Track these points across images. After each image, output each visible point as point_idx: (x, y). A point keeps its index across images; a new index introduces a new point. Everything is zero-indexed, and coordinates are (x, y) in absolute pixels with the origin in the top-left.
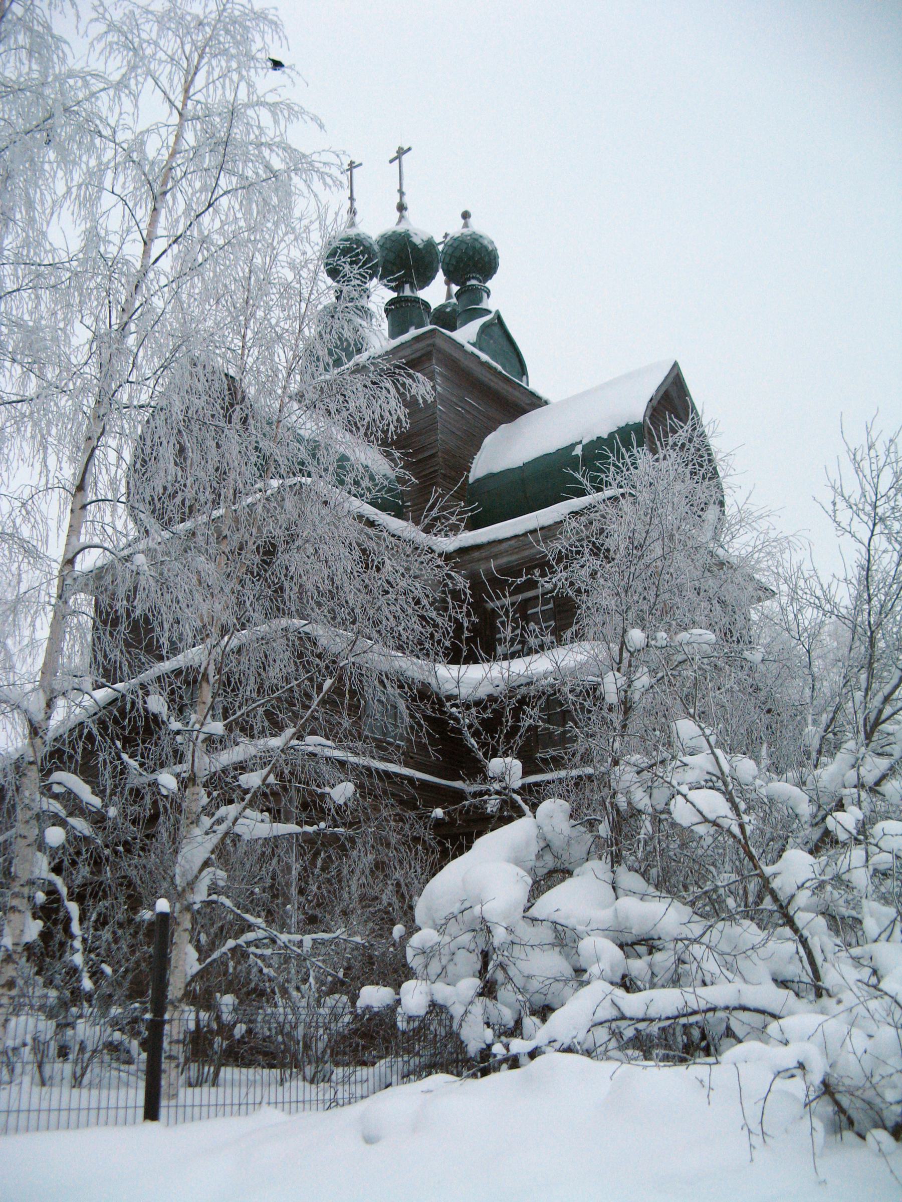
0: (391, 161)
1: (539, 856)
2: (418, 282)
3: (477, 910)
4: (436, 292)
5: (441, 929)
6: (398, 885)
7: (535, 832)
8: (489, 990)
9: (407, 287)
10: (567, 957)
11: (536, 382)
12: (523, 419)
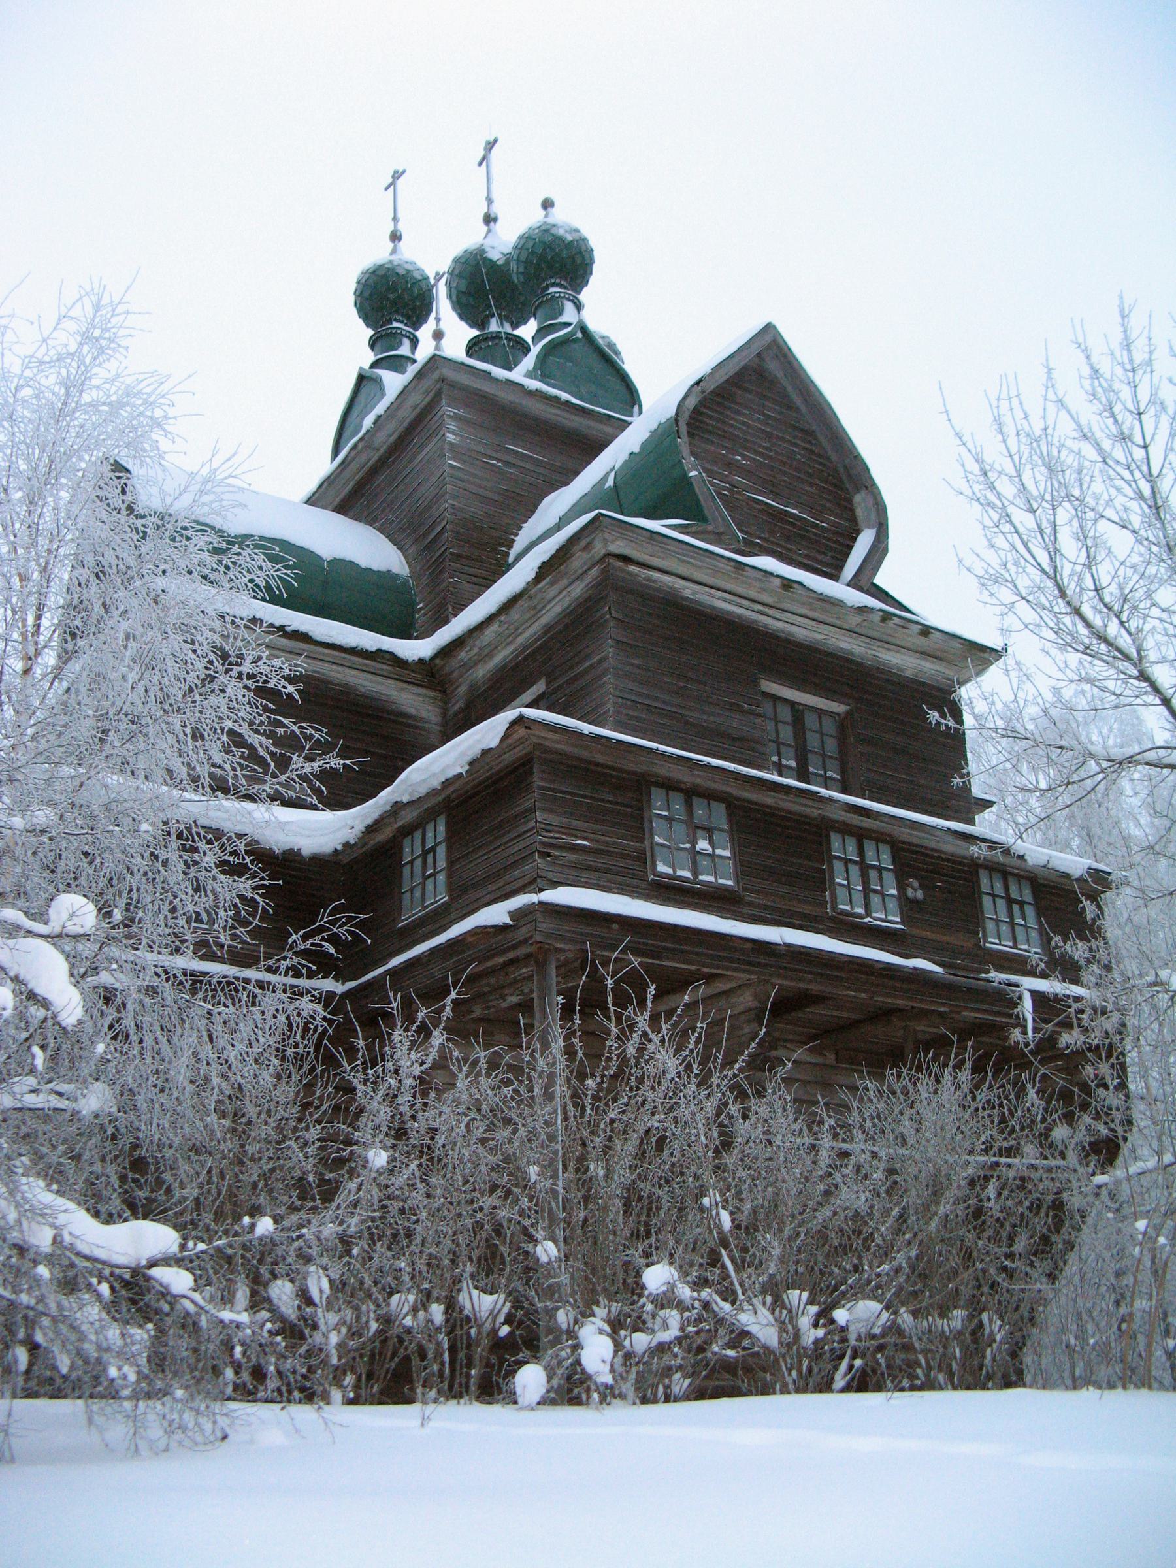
0: (386, 189)
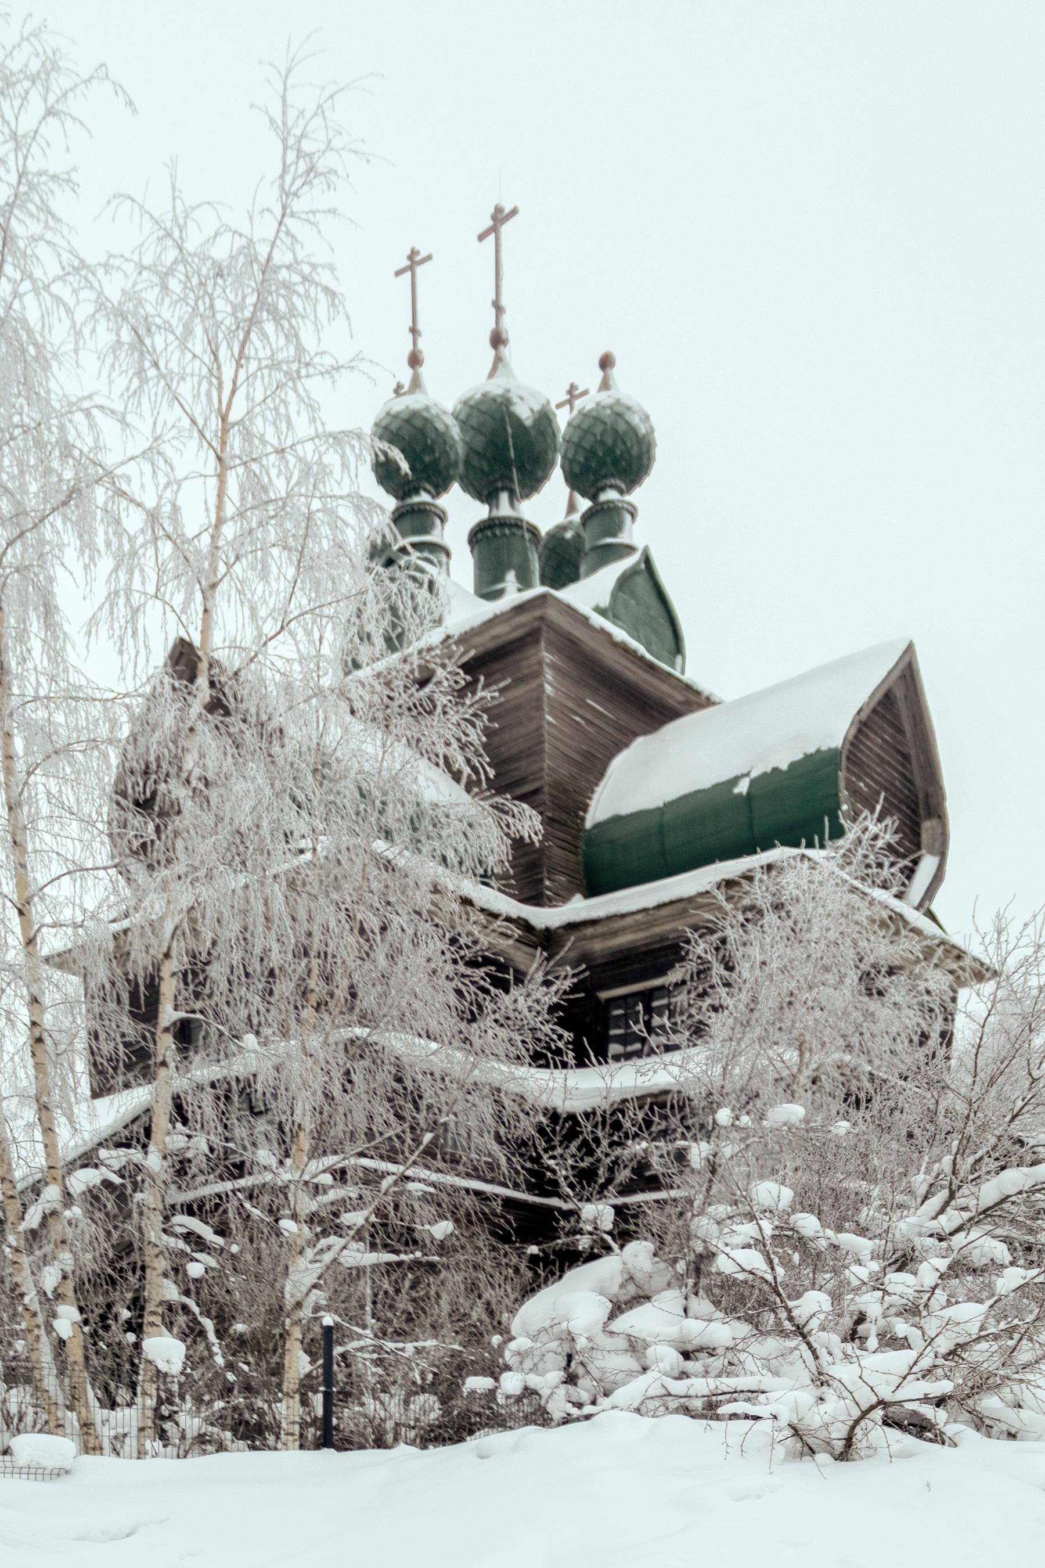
0: (481, 237)
1: (622, 1286)
2: (523, 486)
3: (564, 1325)
4: (550, 506)
5: (534, 1338)
6: (488, 1303)
7: (621, 1267)
8: (571, 1379)
9: (504, 497)
10: (638, 1359)
11: (696, 668)
12: (671, 730)
